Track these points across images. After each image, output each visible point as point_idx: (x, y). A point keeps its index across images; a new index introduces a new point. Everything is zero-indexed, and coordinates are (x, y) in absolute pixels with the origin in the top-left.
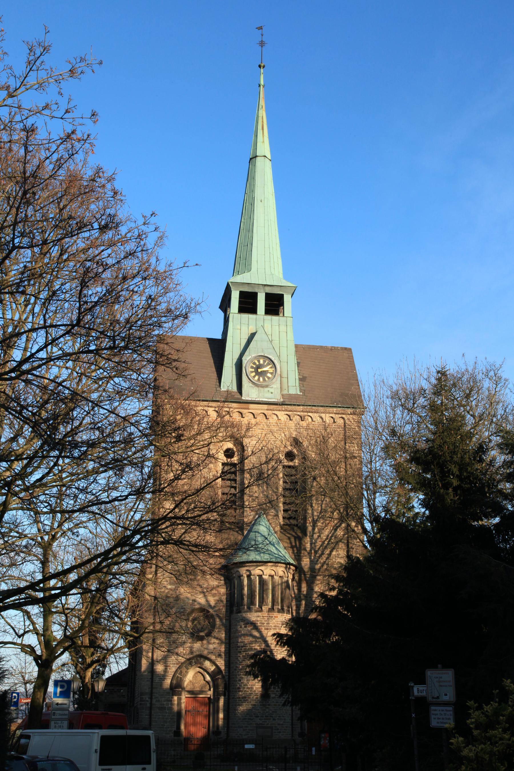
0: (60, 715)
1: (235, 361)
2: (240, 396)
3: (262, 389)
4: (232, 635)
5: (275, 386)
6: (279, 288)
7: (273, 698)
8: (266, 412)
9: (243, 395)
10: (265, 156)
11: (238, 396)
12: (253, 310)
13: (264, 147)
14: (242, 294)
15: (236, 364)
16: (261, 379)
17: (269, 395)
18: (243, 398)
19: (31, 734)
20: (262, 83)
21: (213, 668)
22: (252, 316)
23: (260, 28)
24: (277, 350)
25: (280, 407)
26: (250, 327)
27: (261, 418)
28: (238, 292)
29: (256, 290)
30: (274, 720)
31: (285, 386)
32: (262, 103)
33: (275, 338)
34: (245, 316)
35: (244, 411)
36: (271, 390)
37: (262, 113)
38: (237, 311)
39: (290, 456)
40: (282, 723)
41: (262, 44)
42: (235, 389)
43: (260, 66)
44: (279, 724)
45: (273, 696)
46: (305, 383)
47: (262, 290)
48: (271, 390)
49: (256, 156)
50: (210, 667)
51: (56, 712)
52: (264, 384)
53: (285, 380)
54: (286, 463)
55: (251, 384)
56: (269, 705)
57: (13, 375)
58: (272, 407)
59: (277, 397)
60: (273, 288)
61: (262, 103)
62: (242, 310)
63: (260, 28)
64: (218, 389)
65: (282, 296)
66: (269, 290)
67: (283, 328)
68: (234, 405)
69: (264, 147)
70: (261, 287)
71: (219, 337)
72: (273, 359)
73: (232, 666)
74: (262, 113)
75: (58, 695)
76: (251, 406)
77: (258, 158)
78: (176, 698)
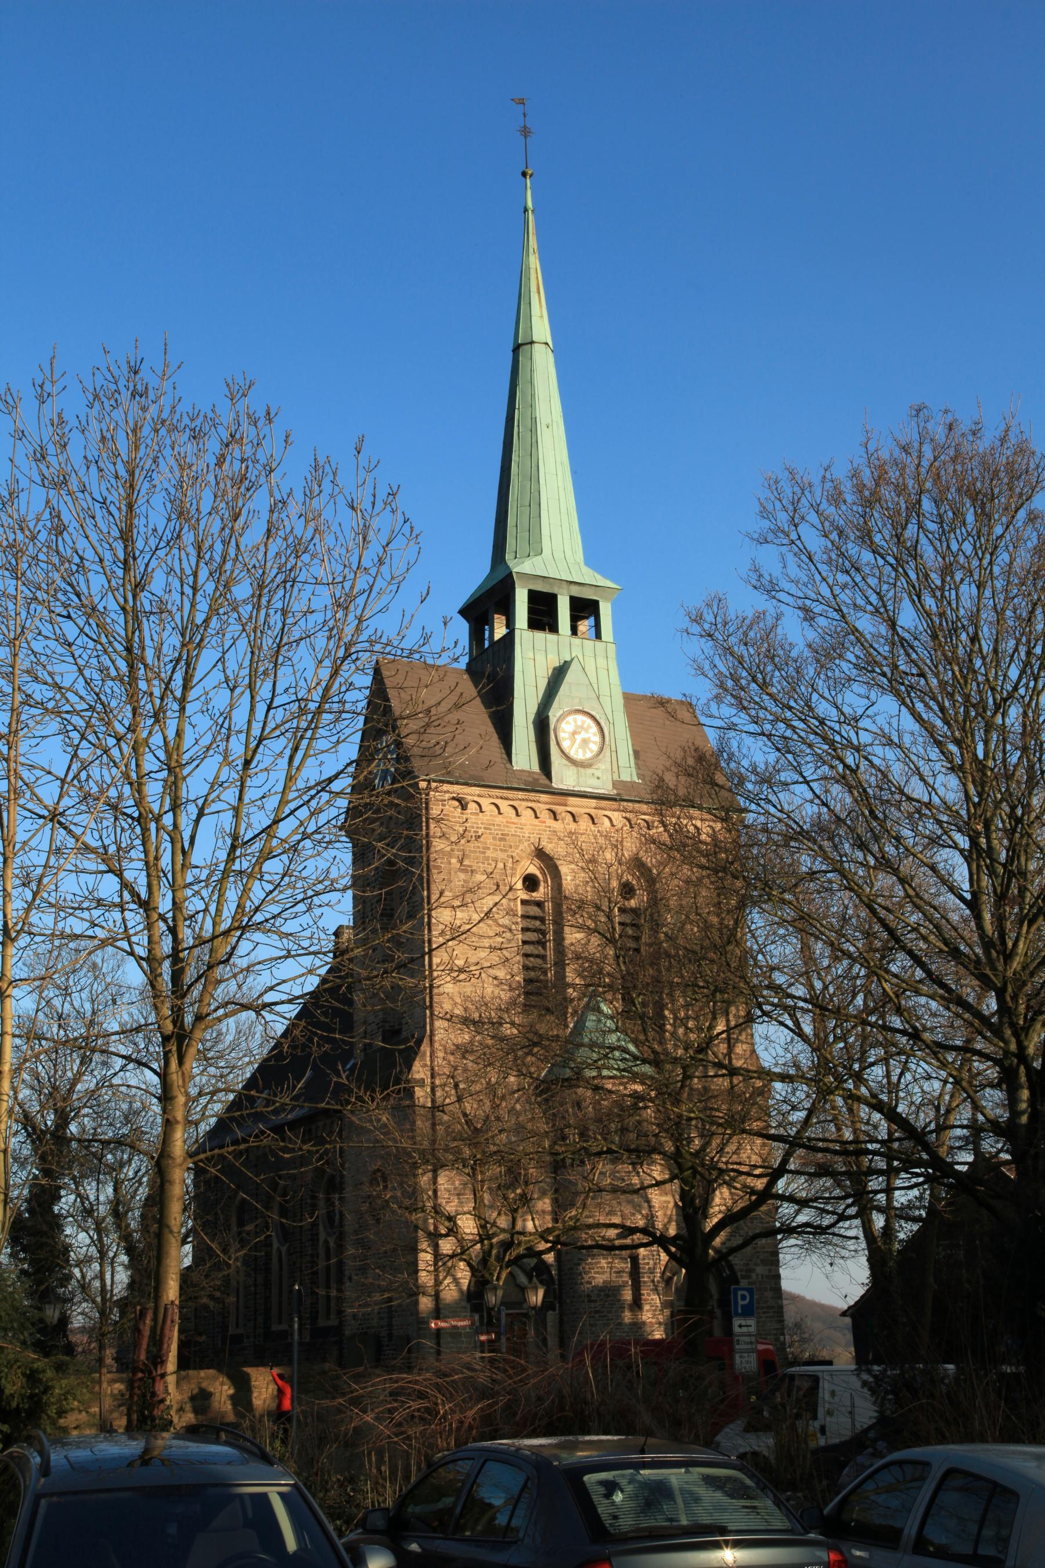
1: (531, 717)
2: (547, 782)
3: (581, 770)
6: (540, 581)
8: (593, 812)
11: (543, 780)
12: (553, 627)
13: (541, 328)
15: (534, 723)
17: (594, 782)
19: (820, 1374)
20: (530, 204)
22: (551, 637)
23: (521, 102)
25: (615, 805)
27: (584, 824)
29: (555, 591)
32: (533, 242)
34: (540, 636)
35: (559, 809)
36: (598, 773)
37: (534, 262)
38: (525, 625)
39: (531, 882)
42: (536, 768)
43: (524, 174)
47: (565, 591)
49: (532, 343)
54: (523, 895)
55: (565, 762)
58: (604, 803)
59: (605, 787)
60: (584, 589)
61: (533, 242)
62: (535, 624)
63: (521, 102)
64: (508, 765)
65: (596, 604)
66: (576, 592)
67: (602, 662)
68: (544, 797)
69: (541, 326)
70: (564, 584)
74: (534, 262)
76: (572, 800)
77: (536, 346)
78: (307, 1339)
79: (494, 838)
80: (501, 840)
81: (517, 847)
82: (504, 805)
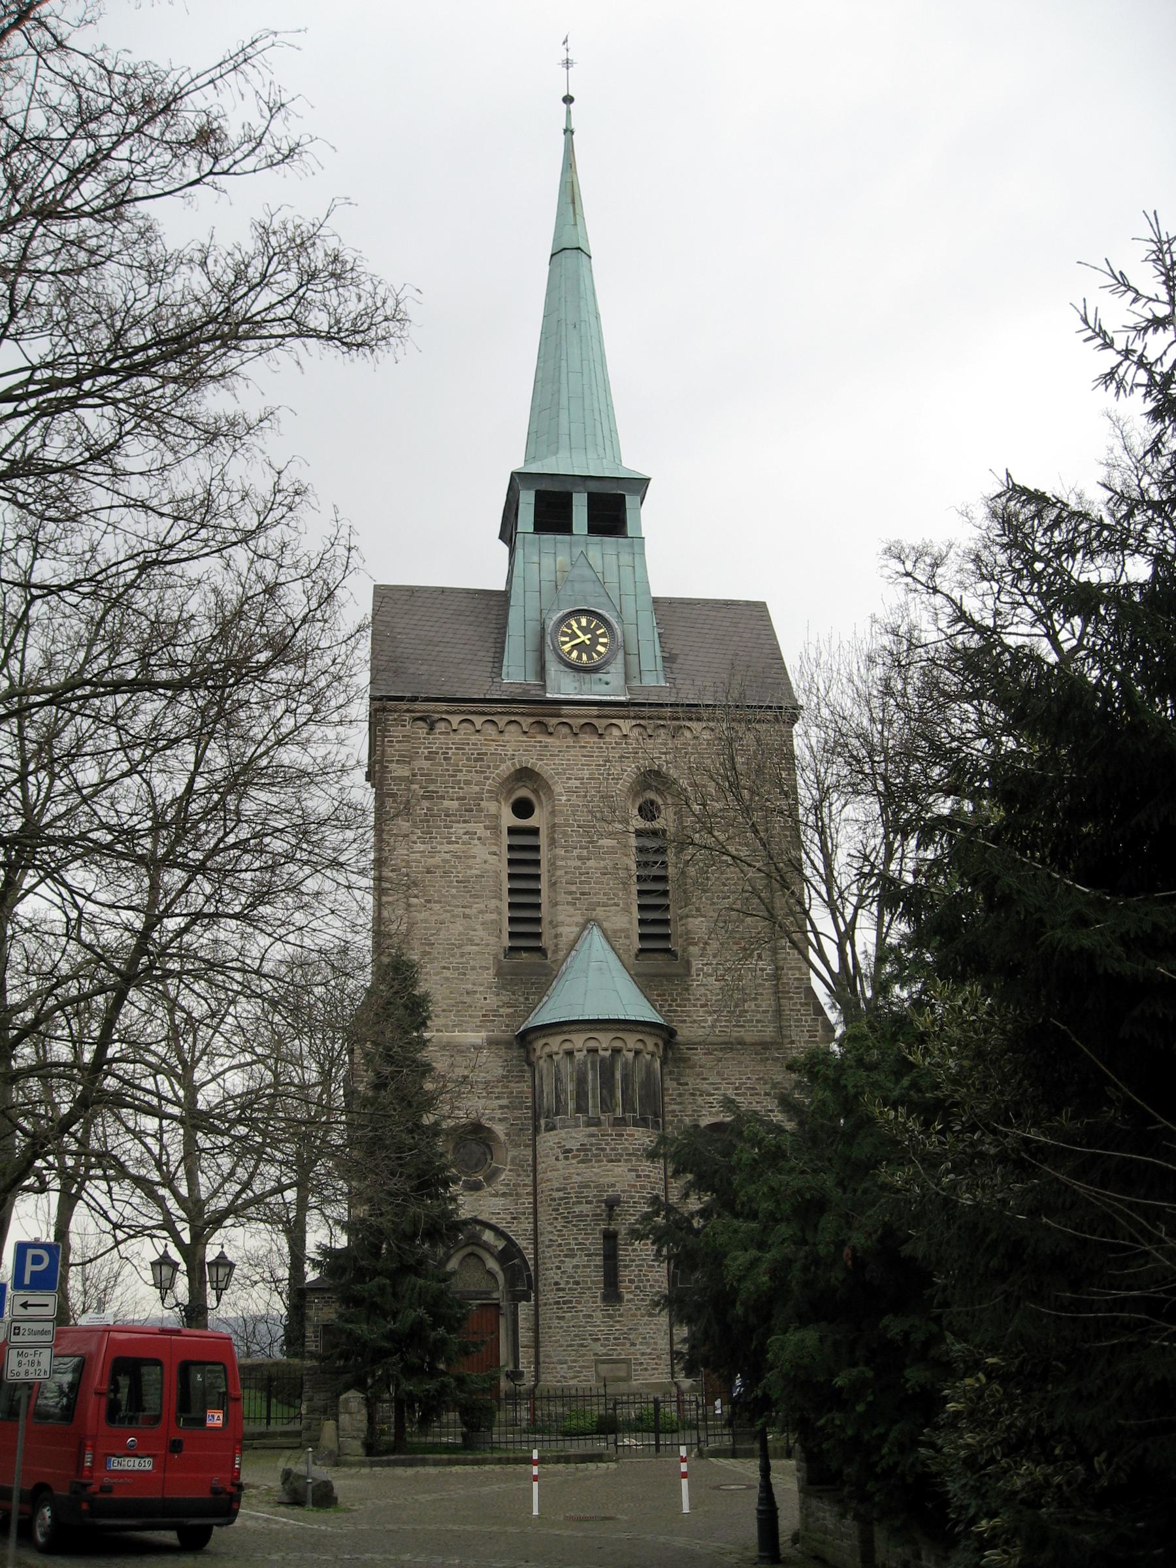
0: (32, 1332)
3: (587, 676)
4: (539, 1177)
5: (614, 675)
7: (629, 1301)
9: (549, 689)
10: (579, 248)
12: (565, 527)
14: (539, 495)
16: (584, 657)
18: (548, 695)
21: (501, 1245)
24: (616, 601)
25: (623, 711)
26: (559, 559)
28: (533, 493)
29: (569, 488)
30: (633, 1344)
31: (634, 670)
33: (611, 578)
40: (648, 1351)
41: (567, 63)
44: (643, 1354)
45: (627, 1297)
46: (675, 666)
48: (605, 677)
50: (497, 1243)
51: (22, 1325)
52: (592, 664)
53: (633, 659)
55: (562, 668)
56: (621, 1316)
57: (102, 690)
66: (594, 487)
71: (502, 587)
72: (607, 615)
73: (540, 1239)
75: (27, 1281)
76: (566, 709)
79: (468, 759)
80: (476, 760)
81: (497, 767)
82: (478, 720)
